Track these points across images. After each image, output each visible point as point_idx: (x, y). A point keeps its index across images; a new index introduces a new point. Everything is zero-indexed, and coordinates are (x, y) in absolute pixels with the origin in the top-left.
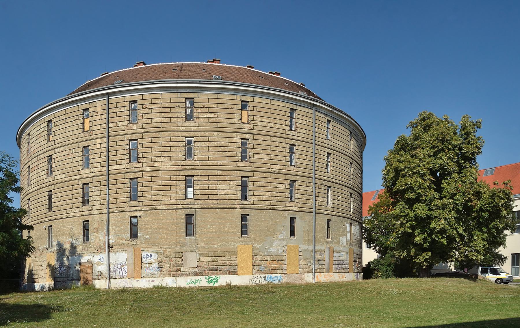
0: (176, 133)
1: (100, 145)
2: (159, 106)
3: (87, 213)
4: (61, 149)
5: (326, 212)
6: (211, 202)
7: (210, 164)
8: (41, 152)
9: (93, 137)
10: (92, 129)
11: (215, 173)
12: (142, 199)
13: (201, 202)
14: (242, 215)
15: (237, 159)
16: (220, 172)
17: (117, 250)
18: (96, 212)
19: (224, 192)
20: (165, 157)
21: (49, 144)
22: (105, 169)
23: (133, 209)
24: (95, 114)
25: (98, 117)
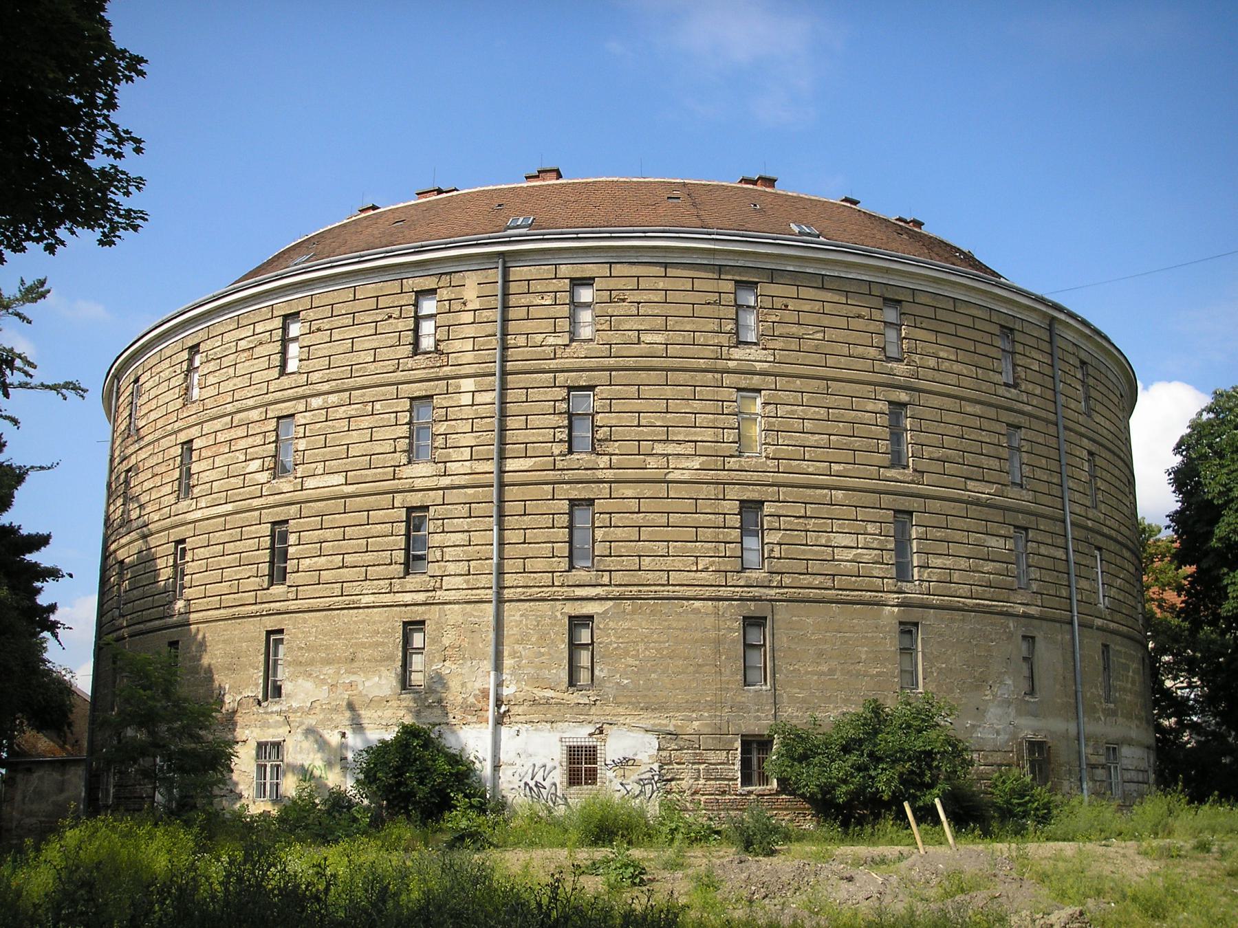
0: (710, 375)
1: (471, 396)
2: (658, 297)
3: (421, 597)
4: (333, 399)
5: (1099, 622)
6: (817, 581)
7: (810, 470)
8: (251, 402)
9: (447, 370)
10: (442, 346)
11: (825, 496)
13: (787, 580)
14: (901, 623)
15: (877, 458)
16: (839, 494)
17: (522, 719)
18: (452, 596)
19: (850, 554)
20: (679, 442)
22: (491, 466)
23: (580, 592)
24: (456, 306)
25: (468, 317)
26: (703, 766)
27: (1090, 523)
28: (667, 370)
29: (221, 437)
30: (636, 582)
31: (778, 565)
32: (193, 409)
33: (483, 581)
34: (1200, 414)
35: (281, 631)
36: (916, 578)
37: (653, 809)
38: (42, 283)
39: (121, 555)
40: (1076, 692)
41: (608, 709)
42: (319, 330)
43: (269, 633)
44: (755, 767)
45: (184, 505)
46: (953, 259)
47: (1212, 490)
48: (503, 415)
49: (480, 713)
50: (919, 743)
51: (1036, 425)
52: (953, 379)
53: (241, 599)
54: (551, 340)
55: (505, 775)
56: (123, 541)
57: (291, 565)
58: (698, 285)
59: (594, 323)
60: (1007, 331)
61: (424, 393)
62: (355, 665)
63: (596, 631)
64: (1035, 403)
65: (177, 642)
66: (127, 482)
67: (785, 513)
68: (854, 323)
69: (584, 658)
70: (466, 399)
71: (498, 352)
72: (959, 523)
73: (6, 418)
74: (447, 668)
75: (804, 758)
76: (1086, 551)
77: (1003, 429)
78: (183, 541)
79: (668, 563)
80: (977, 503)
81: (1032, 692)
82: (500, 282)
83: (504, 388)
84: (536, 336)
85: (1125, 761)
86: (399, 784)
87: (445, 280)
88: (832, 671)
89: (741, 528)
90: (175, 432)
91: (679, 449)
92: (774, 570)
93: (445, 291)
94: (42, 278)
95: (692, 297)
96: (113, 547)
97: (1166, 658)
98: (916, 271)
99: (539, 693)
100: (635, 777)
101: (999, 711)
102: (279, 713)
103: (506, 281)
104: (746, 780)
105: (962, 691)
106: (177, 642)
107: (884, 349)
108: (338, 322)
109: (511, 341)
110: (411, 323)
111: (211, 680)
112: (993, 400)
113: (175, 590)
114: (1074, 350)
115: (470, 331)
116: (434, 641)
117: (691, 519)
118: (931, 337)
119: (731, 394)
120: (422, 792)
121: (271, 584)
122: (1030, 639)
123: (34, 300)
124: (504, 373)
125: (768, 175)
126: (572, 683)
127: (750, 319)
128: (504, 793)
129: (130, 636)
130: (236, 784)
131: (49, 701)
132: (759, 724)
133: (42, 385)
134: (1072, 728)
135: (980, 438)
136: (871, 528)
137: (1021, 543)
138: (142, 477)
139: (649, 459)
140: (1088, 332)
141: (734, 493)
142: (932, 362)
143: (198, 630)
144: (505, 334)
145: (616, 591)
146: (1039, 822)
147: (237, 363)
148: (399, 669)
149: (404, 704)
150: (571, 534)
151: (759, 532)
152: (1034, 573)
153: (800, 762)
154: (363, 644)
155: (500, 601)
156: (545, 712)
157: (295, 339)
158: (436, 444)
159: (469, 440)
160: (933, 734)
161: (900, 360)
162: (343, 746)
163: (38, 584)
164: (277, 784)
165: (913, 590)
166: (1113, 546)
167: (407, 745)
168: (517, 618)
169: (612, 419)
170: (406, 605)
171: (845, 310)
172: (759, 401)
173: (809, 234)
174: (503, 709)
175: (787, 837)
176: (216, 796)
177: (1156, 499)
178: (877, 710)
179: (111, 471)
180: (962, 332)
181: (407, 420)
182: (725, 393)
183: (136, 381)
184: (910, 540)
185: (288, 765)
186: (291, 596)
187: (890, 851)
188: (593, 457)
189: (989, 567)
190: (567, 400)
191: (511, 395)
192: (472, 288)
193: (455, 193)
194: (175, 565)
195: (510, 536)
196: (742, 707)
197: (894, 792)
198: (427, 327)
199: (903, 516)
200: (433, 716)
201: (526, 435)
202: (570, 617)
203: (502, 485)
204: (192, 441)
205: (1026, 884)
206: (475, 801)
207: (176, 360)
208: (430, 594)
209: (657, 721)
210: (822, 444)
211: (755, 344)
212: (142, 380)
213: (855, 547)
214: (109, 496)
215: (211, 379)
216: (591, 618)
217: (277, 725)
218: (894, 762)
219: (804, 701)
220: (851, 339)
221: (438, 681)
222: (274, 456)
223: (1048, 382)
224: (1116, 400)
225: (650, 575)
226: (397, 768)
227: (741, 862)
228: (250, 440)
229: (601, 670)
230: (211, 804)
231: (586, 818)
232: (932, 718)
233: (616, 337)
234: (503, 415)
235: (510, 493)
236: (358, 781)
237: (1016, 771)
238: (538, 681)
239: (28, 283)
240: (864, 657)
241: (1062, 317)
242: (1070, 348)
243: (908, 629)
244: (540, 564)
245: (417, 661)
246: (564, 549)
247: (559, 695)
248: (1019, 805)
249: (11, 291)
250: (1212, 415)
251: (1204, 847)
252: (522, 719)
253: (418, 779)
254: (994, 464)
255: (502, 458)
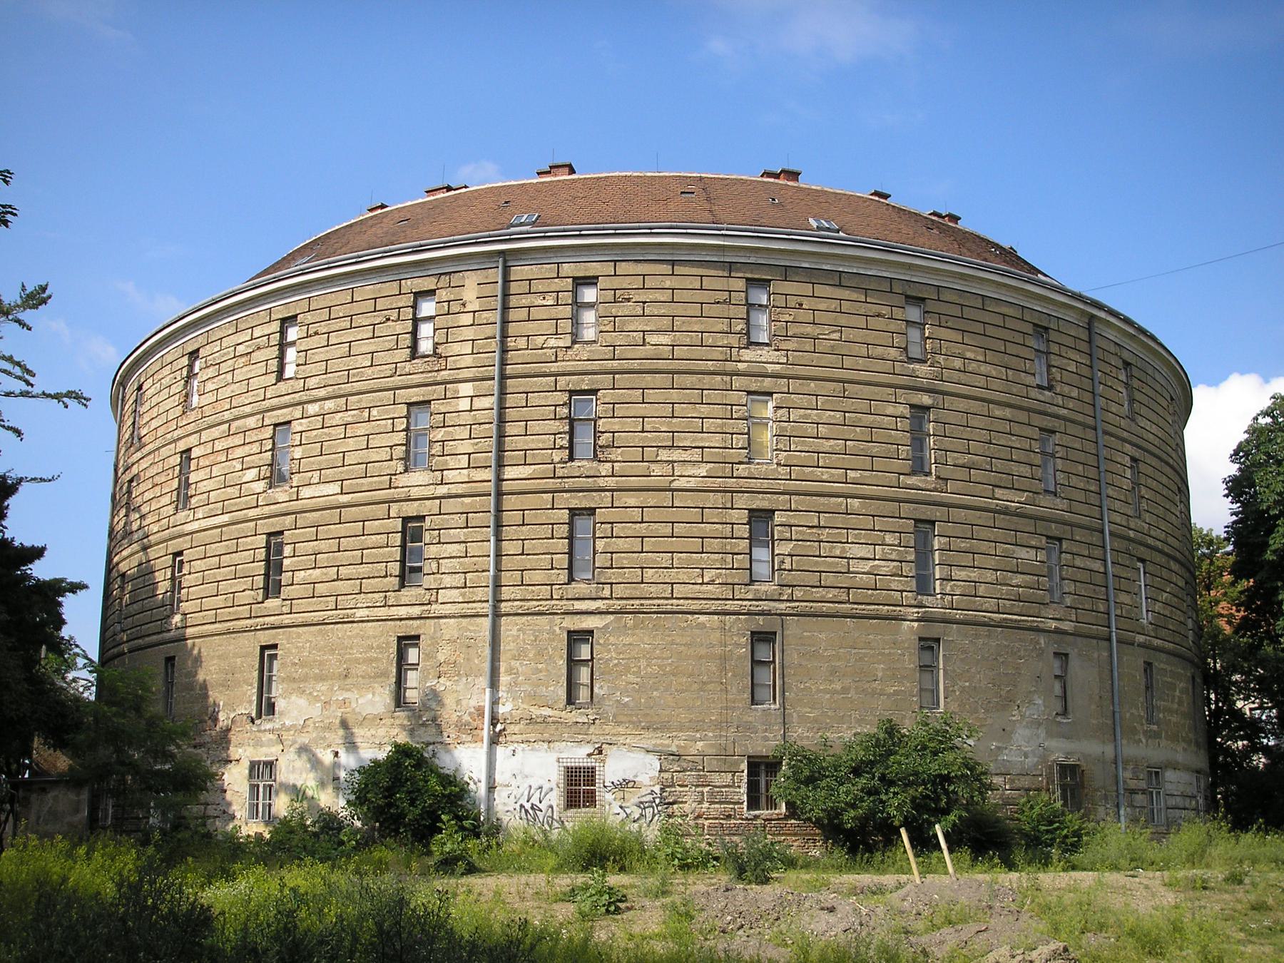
0: (719, 378)
1: (470, 400)
2: (666, 296)
3: (416, 611)
4: (329, 405)
5: (1141, 638)
6: (830, 594)
7: (824, 477)
8: (248, 409)
12: (611, 575)
13: (798, 593)
14: (921, 639)
16: (856, 503)
17: (519, 738)
20: (685, 448)
21: (283, 387)
22: (489, 474)
24: (455, 307)
25: (467, 319)
26: (707, 789)
27: (1132, 534)
28: (673, 373)
29: (219, 445)
30: (638, 594)
31: (788, 578)
32: (192, 416)
33: (480, 594)
34: (1256, 419)
35: (275, 646)
36: (938, 591)
37: (652, 834)
38: (44, 289)
39: (123, 567)
40: (1114, 712)
41: (607, 729)
42: (316, 333)
43: (263, 648)
44: (763, 790)
45: (182, 515)
46: (987, 255)
47: (1268, 499)
48: (502, 421)
49: (475, 732)
50: (934, 766)
51: (1072, 429)
52: (981, 381)
53: (235, 613)
54: (552, 342)
55: (500, 797)
56: (125, 553)
57: (285, 578)
58: (707, 283)
59: (597, 324)
60: (1041, 330)
61: (421, 399)
62: (349, 681)
63: (595, 646)
64: (1071, 406)
65: (173, 658)
66: (129, 492)
67: (796, 522)
68: (873, 322)
69: (584, 674)
70: (464, 404)
71: (497, 355)
72: (986, 533)
73: (9, 428)
74: (442, 685)
75: (811, 781)
76: (1127, 563)
77: (1036, 433)
78: (180, 553)
79: (673, 575)
80: (1005, 512)
81: (1065, 713)
82: (500, 282)
83: (503, 393)
84: (538, 337)
85: (1168, 786)
86: (390, 805)
87: (444, 281)
88: (845, 690)
89: (750, 538)
90: (175, 441)
91: (685, 456)
92: (785, 582)
93: (443, 292)
94: (43, 284)
95: (700, 297)
96: (115, 560)
97: (1237, 677)
98: (938, 266)
99: (536, 712)
100: (636, 800)
101: (1027, 732)
102: (271, 731)
103: (506, 281)
104: (753, 803)
105: (987, 711)
106: (173, 658)
107: (906, 349)
108: (335, 325)
109: (511, 343)
110: (409, 326)
111: (206, 696)
112: (1026, 403)
113: (171, 605)
114: (1118, 350)
115: (469, 333)
116: (429, 656)
117: (696, 529)
118: (957, 337)
119: (741, 397)
120: (413, 813)
121: (266, 597)
122: (1063, 656)
123: (35, 307)
124: (503, 377)
125: (791, 168)
126: (571, 700)
127: (762, 319)
128: (499, 815)
129: (130, 652)
130: (229, 804)
131: (62, 719)
132: (765, 745)
133: (44, 393)
134: (1109, 750)
135: (1010, 444)
136: (889, 539)
137: (1055, 555)
138: (142, 487)
139: (653, 466)
140: (1131, 331)
141: (742, 501)
142: (958, 363)
143: (194, 645)
144: (504, 336)
145: (617, 605)
146: (1066, 851)
147: (236, 371)
148: (393, 686)
149: (398, 722)
150: (571, 545)
151: (771, 543)
152: (1069, 587)
153: (807, 786)
154: (357, 660)
155: (497, 615)
156: (542, 731)
157: (293, 343)
158: (433, 452)
159: (467, 447)
160: (950, 757)
161: (924, 362)
162: (336, 765)
163: (60, 599)
164: (270, 805)
165: (934, 605)
166: (1159, 558)
167: (399, 765)
168: (514, 632)
169: (615, 424)
170: (401, 620)
171: (863, 309)
172: (771, 405)
173: (828, 229)
174: (499, 727)
175: (791, 863)
176: (209, 817)
177: (1212, 511)
178: (891, 730)
179: (116, 482)
180: (991, 331)
181: (404, 426)
182: (734, 397)
183: (140, 388)
184: (932, 551)
185: (281, 784)
186: (286, 610)
187: (889, 879)
188: (595, 464)
189: (1018, 579)
190: (568, 404)
191: (511, 400)
192: (472, 288)
193: (464, 190)
194: (173, 578)
195: (508, 547)
196: (749, 728)
197: (906, 818)
198: (426, 330)
199: (924, 526)
200: (427, 735)
201: (525, 441)
202: (569, 632)
203: (500, 494)
204: (190, 449)
205: (1025, 917)
206: (467, 823)
207: (177, 365)
208: (425, 608)
209: (659, 742)
210: (837, 449)
211: (767, 345)
212: (145, 387)
213: (872, 558)
214: (114, 507)
215: (210, 386)
216: (591, 632)
217: (270, 744)
218: (906, 785)
219: (815, 720)
220: (870, 339)
221: (434, 696)
222: (271, 465)
223: (1086, 384)
224: (1165, 404)
225: (653, 588)
226: (387, 789)
227: (727, 890)
228: (247, 448)
229: (601, 687)
230: (204, 825)
231: (578, 842)
232: (950, 739)
233: (619, 339)
234: (502, 421)
235: (509, 502)
236: (348, 802)
237: (1045, 796)
238: (534, 699)
239: (29, 289)
240: (880, 674)
241: (1102, 315)
242: (1112, 348)
243: (928, 644)
244: (538, 577)
245: (412, 678)
246: (562, 560)
247: (557, 713)
248: (1048, 831)
249: (11, 297)
250: (1268, 420)
251: (1235, 879)
252: (519, 738)
253: (411, 801)
254: (1026, 470)
255: (500, 465)
